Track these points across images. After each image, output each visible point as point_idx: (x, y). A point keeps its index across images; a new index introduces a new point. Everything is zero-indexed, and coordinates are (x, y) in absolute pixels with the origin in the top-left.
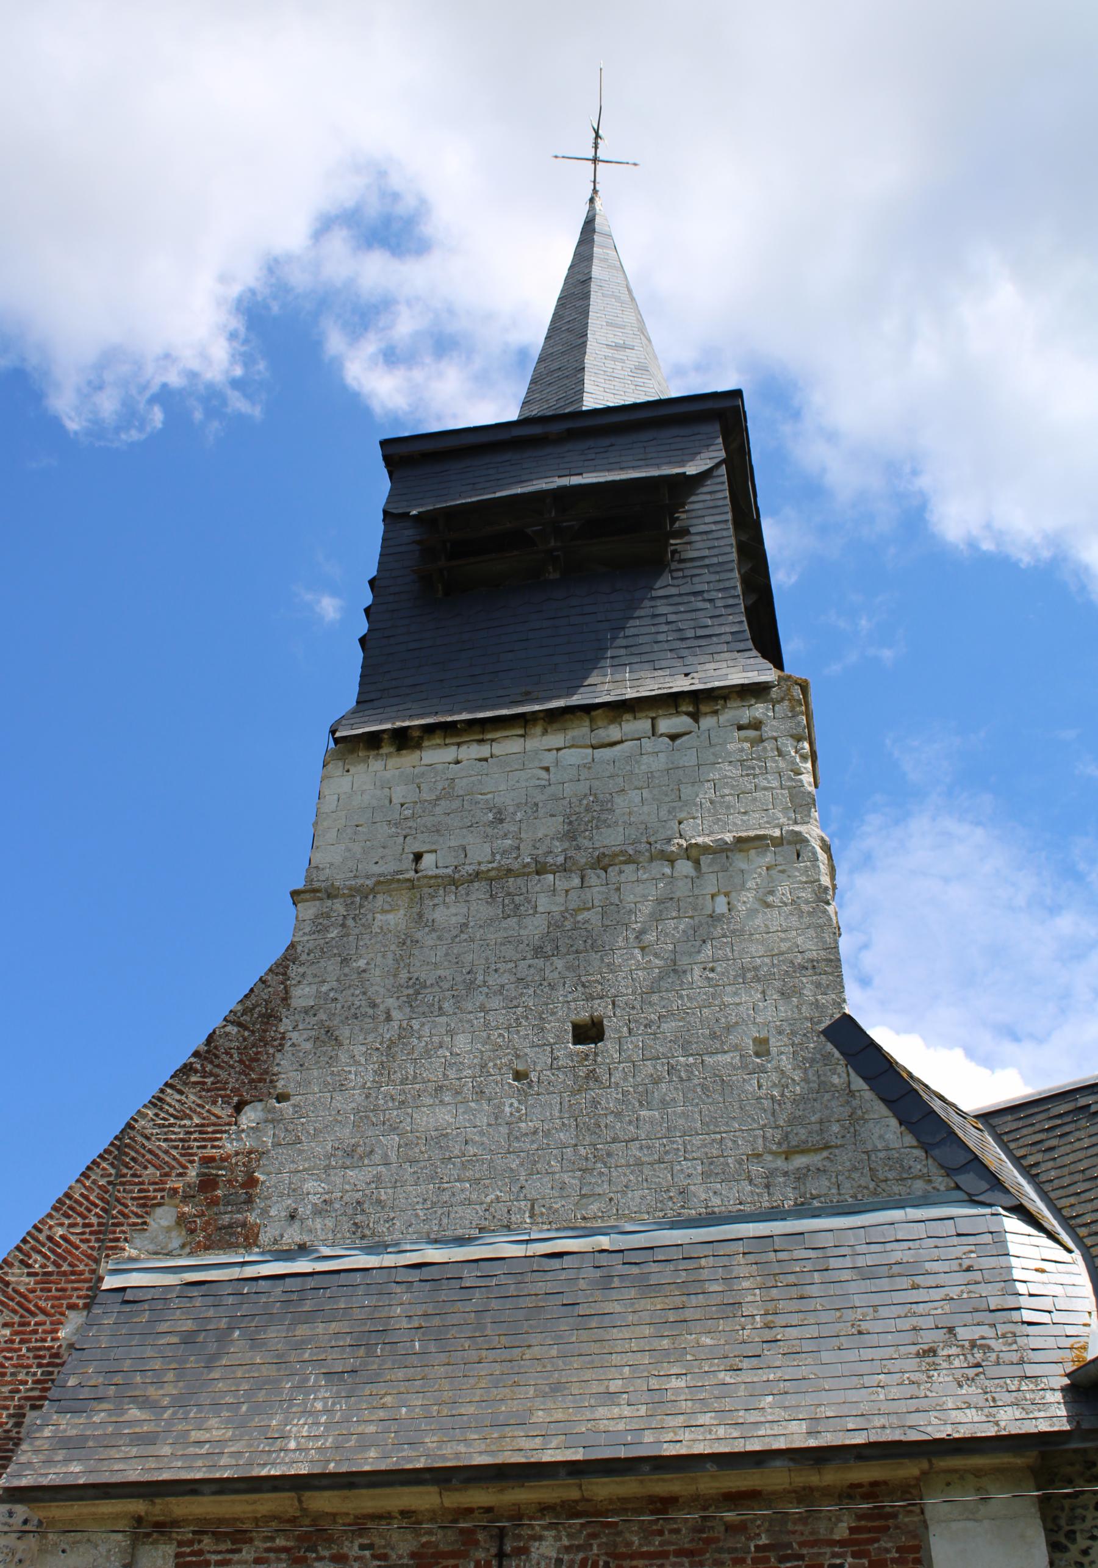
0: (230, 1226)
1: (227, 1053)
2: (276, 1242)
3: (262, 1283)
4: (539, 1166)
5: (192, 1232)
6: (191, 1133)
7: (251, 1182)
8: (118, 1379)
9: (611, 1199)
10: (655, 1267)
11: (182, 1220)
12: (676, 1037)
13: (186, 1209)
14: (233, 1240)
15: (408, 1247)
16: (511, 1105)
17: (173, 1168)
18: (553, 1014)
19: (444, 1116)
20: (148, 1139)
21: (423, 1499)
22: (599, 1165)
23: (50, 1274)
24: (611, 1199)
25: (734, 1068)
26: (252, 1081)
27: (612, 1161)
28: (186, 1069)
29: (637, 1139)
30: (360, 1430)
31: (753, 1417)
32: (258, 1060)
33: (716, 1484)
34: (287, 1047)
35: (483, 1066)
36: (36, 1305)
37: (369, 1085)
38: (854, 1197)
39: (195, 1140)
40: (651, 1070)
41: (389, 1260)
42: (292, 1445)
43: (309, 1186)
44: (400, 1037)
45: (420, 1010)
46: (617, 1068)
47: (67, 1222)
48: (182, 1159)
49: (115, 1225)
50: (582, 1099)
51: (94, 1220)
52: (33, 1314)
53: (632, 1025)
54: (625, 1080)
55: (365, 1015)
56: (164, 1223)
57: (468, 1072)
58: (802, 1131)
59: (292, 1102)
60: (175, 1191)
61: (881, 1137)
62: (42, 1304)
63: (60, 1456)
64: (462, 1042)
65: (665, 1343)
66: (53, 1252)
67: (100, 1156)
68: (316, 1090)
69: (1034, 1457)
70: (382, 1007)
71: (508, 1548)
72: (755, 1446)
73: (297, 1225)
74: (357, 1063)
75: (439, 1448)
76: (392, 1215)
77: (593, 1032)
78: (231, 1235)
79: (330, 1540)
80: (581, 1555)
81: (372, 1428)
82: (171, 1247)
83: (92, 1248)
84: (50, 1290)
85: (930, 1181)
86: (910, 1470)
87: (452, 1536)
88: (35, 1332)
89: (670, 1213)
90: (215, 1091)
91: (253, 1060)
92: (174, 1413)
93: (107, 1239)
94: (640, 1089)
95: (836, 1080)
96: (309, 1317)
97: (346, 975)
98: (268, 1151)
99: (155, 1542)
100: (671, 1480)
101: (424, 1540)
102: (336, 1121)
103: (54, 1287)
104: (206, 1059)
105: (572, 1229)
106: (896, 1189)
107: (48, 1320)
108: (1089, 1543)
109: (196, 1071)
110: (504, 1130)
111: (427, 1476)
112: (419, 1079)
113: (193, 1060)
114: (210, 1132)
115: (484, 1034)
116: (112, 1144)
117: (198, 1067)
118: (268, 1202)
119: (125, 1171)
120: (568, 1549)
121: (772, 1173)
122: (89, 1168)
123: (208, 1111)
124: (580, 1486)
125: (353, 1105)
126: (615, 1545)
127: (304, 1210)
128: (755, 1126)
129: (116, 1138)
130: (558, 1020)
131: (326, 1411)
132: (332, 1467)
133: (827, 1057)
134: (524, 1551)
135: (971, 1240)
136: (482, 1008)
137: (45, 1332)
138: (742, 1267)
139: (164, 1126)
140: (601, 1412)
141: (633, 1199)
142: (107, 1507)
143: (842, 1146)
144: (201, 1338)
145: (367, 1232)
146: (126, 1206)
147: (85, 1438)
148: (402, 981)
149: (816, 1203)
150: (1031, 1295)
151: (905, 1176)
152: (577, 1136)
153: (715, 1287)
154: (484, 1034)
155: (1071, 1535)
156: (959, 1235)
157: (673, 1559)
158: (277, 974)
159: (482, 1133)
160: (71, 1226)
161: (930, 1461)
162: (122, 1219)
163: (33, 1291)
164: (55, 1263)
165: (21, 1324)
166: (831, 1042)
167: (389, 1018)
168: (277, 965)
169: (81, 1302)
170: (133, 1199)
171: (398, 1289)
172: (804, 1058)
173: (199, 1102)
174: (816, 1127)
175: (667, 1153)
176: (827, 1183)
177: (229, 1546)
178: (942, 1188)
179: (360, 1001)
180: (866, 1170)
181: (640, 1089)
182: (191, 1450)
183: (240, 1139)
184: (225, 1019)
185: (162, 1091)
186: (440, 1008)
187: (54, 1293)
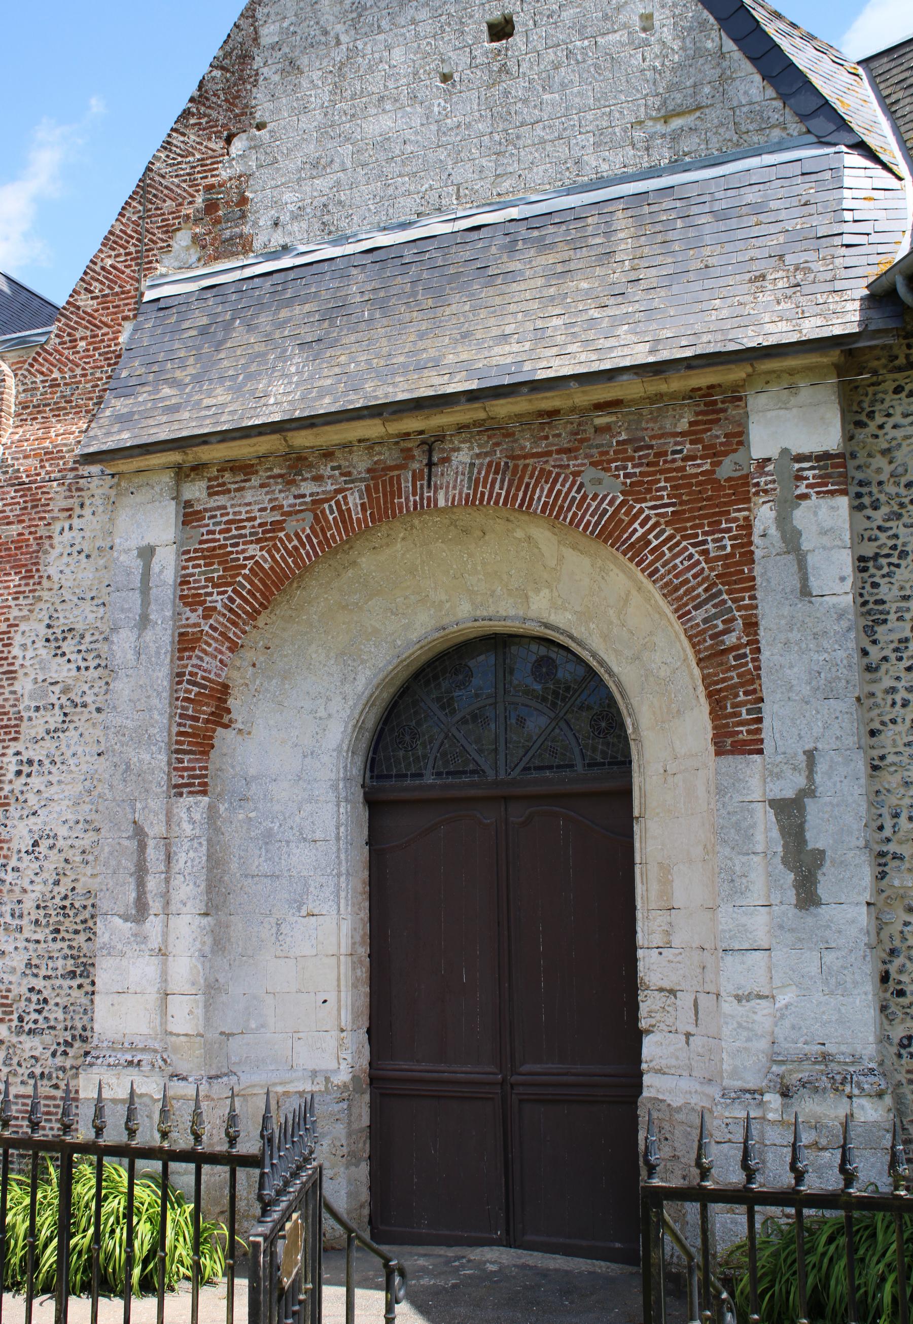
0: (231, 239)
1: (215, 95)
2: (265, 246)
3: (256, 280)
4: (462, 155)
5: (204, 247)
6: (194, 167)
7: (243, 200)
8: (155, 368)
9: (520, 176)
10: (551, 229)
11: (195, 238)
12: (574, 23)
13: (197, 230)
14: (234, 249)
15: (364, 237)
16: (439, 105)
17: (185, 198)
18: (471, 17)
19: (386, 122)
20: (163, 177)
21: (372, 429)
22: (510, 148)
23: (106, 296)
24: (520, 176)
25: (623, 45)
26: (236, 116)
27: (520, 143)
28: (186, 114)
29: (541, 121)
30: (320, 383)
31: (612, 342)
32: (238, 97)
33: (586, 398)
34: (261, 82)
35: (416, 74)
36: (101, 321)
37: (326, 104)
38: (720, 150)
39: (199, 172)
40: (552, 57)
41: (349, 249)
42: (272, 401)
43: (288, 197)
44: (348, 58)
45: (363, 31)
46: (524, 60)
47: (113, 253)
48: (190, 190)
49: (147, 251)
50: (496, 91)
51: (132, 249)
52: (99, 328)
53: (537, 18)
54: (531, 68)
55: (319, 43)
56: (184, 244)
57: (404, 81)
58: (678, 96)
59: (268, 128)
60: (187, 216)
61: (746, 93)
62: (104, 319)
63: (116, 428)
64: (398, 55)
65: (552, 291)
66: (107, 278)
67: (131, 197)
68: (286, 115)
69: (843, 361)
70: (332, 34)
71: (435, 459)
72: (607, 365)
73: (280, 229)
74: (316, 87)
75: (374, 391)
76: (350, 212)
77: (508, 30)
78: (232, 245)
79: (310, 466)
80: (488, 459)
81: (329, 382)
82: (190, 262)
83: (134, 271)
84: (108, 308)
85: (785, 128)
86: (737, 374)
87: (396, 454)
88: (103, 341)
89: (567, 182)
90: (209, 129)
91: (235, 98)
92: (193, 388)
93: (143, 262)
94: (544, 75)
95: (709, 45)
96: (289, 303)
97: (301, 9)
98: (254, 173)
99: (193, 480)
100: (553, 397)
101: (376, 459)
102: (303, 139)
103: (111, 305)
104: (200, 102)
105: (489, 204)
106: (755, 139)
107: (110, 330)
108: (885, 419)
109: (193, 115)
110: (434, 127)
111: (365, 412)
112: (365, 93)
113: (190, 105)
114: (208, 165)
115: (415, 45)
116: (138, 186)
117: (195, 110)
118: (257, 215)
119: (150, 206)
120: (478, 456)
121: (652, 137)
122: (123, 208)
123: (206, 147)
124: (485, 409)
125: (315, 124)
126: (513, 450)
127: (285, 218)
128: (639, 96)
129: (140, 180)
130: (475, 23)
131: (298, 373)
132: (297, 414)
133: (703, 24)
134: (447, 460)
135: (813, 177)
136: (414, 22)
137: (109, 340)
138: (621, 221)
139: (174, 165)
140: (497, 350)
141: (537, 173)
142: (156, 460)
143: (712, 105)
144: (212, 330)
145: (333, 229)
146: (154, 234)
147: (132, 413)
148: (347, 7)
149: (687, 159)
150: (855, 221)
151: (764, 126)
152: (492, 125)
153: (598, 240)
154: (415, 45)
155: (871, 415)
156: (803, 174)
157: (555, 456)
158: (247, 18)
159: (417, 133)
160: (117, 256)
161: (752, 365)
162: (152, 246)
163: (97, 311)
164: (109, 287)
165: (93, 337)
166: (708, 9)
167: (338, 43)
168: (247, 9)
169: (131, 314)
170: (158, 228)
171: (354, 271)
172: (683, 28)
173: (198, 140)
174: (690, 91)
175: (565, 129)
176: (697, 140)
177: (243, 478)
178: (795, 134)
179: (315, 31)
180: (731, 125)
181: (544, 75)
182: (204, 413)
183: (231, 167)
184: (211, 66)
185: (169, 136)
186: (379, 27)
187: (112, 310)
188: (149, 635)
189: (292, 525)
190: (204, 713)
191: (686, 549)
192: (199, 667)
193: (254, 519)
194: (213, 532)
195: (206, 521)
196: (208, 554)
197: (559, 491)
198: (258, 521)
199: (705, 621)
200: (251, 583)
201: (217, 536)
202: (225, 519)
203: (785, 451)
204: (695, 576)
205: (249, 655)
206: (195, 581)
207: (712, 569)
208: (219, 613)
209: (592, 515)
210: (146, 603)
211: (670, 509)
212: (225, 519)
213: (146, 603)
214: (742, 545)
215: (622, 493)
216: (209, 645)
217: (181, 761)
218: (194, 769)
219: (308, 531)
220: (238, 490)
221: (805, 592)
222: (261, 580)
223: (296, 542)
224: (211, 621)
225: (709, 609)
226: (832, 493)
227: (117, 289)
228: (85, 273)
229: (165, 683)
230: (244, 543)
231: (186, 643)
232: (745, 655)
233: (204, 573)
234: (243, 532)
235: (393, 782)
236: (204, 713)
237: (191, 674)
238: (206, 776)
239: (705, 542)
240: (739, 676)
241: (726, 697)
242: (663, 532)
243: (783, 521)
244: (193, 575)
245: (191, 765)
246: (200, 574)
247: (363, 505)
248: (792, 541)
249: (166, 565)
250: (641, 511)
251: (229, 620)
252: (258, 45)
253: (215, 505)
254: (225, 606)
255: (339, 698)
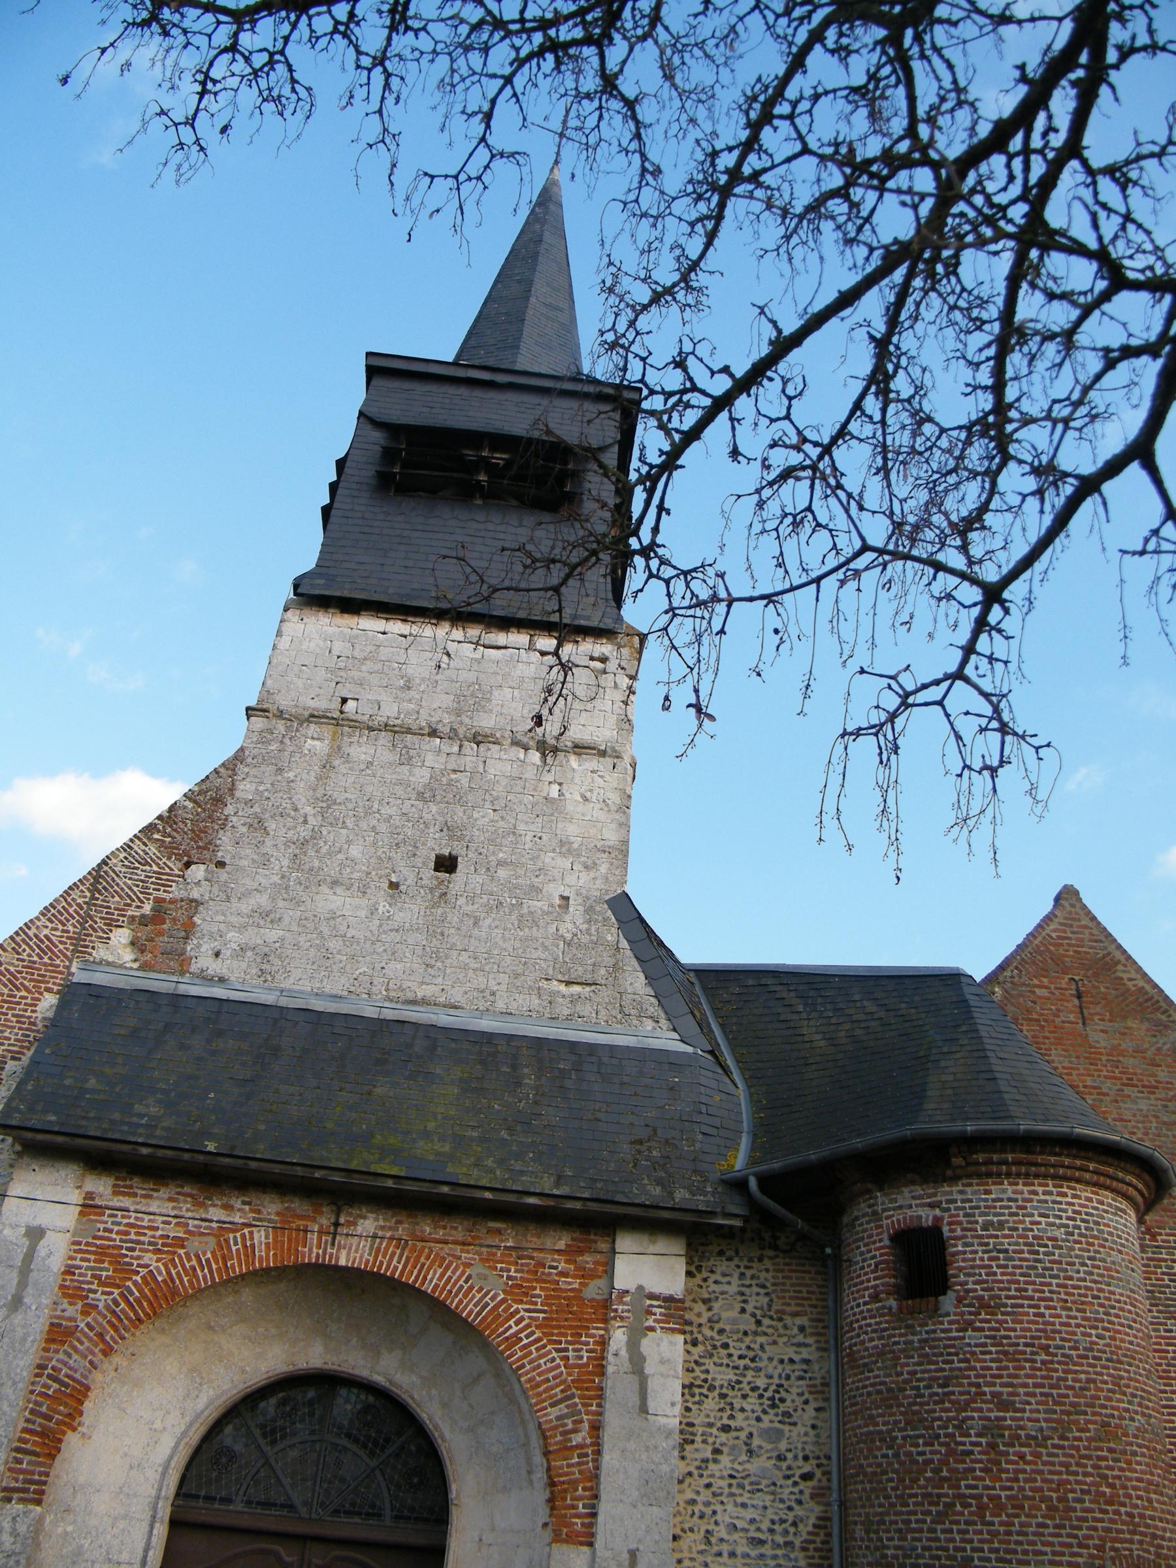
51: (71, 929)
52: (18, 989)
88: (19, 1003)
90: (170, 850)
95: (609, 938)
120: (382, 1228)
167: (305, 822)
188: (18, 1318)
189: (194, 1244)
190: (59, 1413)
191: (550, 1352)
192: (65, 1364)
193: (157, 1229)
194: (111, 1231)
195: (105, 1218)
196: (103, 1253)
197: (450, 1278)
198: (160, 1233)
199: (559, 1418)
200: (140, 1291)
201: (114, 1236)
202: (125, 1221)
203: (640, 1288)
204: (555, 1378)
205: (116, 1359)
206: (80, 1275)
207: (569, 1374)
208: (100, 1313)
209: (475, 1305)
210: (23, 1284)
211: (542, 1315)
212: (125, 1221)
213: (23, 1284)
214: (596, 1359)
215: (504, 1291)
216: (82, 1343)
217: (19, 1461)
218: (33, 1473)
219: (209, 1255)
220: (143, 1196)
221: (643, 1409)
222: (151, 1290)
223: (194, 1262)
224: (89, 1319)
225: (562, 1409)
226: (673, 1330)
227: (46, 960)
228: (17, 933)
229: (25, 1374)
230: (141, 1250)
231: (58, 1334)
232: (587, 1455)
233: (92, 1269)
234: (142, 1238)
235: (201, 1503)
236: (59, 1413)
237: (53, 1368)
238: (45, 1483)
239: (566, 1350)
240: (580, 1472)
241: (565, 1491)
242: (533, 1333)
243: (633, 1345)
244: (80, 1268)
245: (30, 1468)
246: (88, 1268)
247: (267, 1244)
248: (637, 1362)
249: (55, 1251)
250: (517, 1311)
251: (109, 1322)
252: (232, 796)
253: (118, 1204)
254: (107, 1307)
255: (178, 1413)
